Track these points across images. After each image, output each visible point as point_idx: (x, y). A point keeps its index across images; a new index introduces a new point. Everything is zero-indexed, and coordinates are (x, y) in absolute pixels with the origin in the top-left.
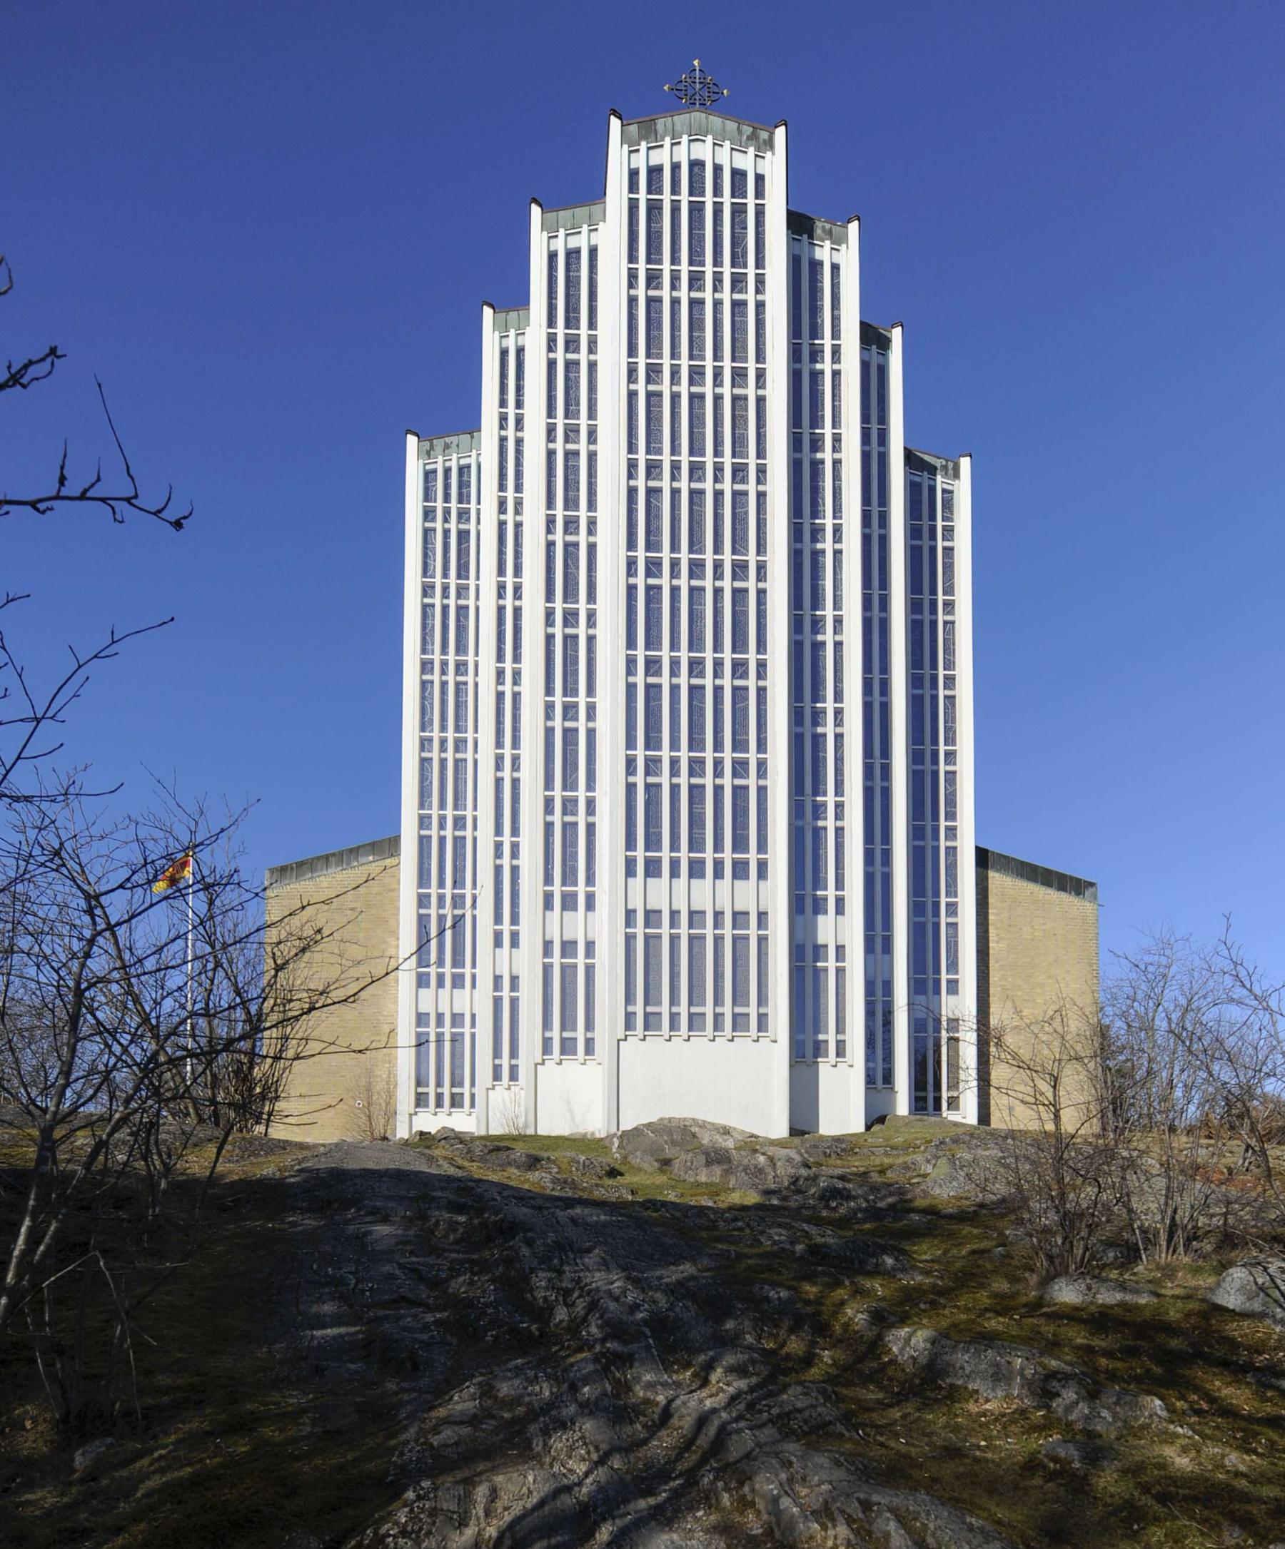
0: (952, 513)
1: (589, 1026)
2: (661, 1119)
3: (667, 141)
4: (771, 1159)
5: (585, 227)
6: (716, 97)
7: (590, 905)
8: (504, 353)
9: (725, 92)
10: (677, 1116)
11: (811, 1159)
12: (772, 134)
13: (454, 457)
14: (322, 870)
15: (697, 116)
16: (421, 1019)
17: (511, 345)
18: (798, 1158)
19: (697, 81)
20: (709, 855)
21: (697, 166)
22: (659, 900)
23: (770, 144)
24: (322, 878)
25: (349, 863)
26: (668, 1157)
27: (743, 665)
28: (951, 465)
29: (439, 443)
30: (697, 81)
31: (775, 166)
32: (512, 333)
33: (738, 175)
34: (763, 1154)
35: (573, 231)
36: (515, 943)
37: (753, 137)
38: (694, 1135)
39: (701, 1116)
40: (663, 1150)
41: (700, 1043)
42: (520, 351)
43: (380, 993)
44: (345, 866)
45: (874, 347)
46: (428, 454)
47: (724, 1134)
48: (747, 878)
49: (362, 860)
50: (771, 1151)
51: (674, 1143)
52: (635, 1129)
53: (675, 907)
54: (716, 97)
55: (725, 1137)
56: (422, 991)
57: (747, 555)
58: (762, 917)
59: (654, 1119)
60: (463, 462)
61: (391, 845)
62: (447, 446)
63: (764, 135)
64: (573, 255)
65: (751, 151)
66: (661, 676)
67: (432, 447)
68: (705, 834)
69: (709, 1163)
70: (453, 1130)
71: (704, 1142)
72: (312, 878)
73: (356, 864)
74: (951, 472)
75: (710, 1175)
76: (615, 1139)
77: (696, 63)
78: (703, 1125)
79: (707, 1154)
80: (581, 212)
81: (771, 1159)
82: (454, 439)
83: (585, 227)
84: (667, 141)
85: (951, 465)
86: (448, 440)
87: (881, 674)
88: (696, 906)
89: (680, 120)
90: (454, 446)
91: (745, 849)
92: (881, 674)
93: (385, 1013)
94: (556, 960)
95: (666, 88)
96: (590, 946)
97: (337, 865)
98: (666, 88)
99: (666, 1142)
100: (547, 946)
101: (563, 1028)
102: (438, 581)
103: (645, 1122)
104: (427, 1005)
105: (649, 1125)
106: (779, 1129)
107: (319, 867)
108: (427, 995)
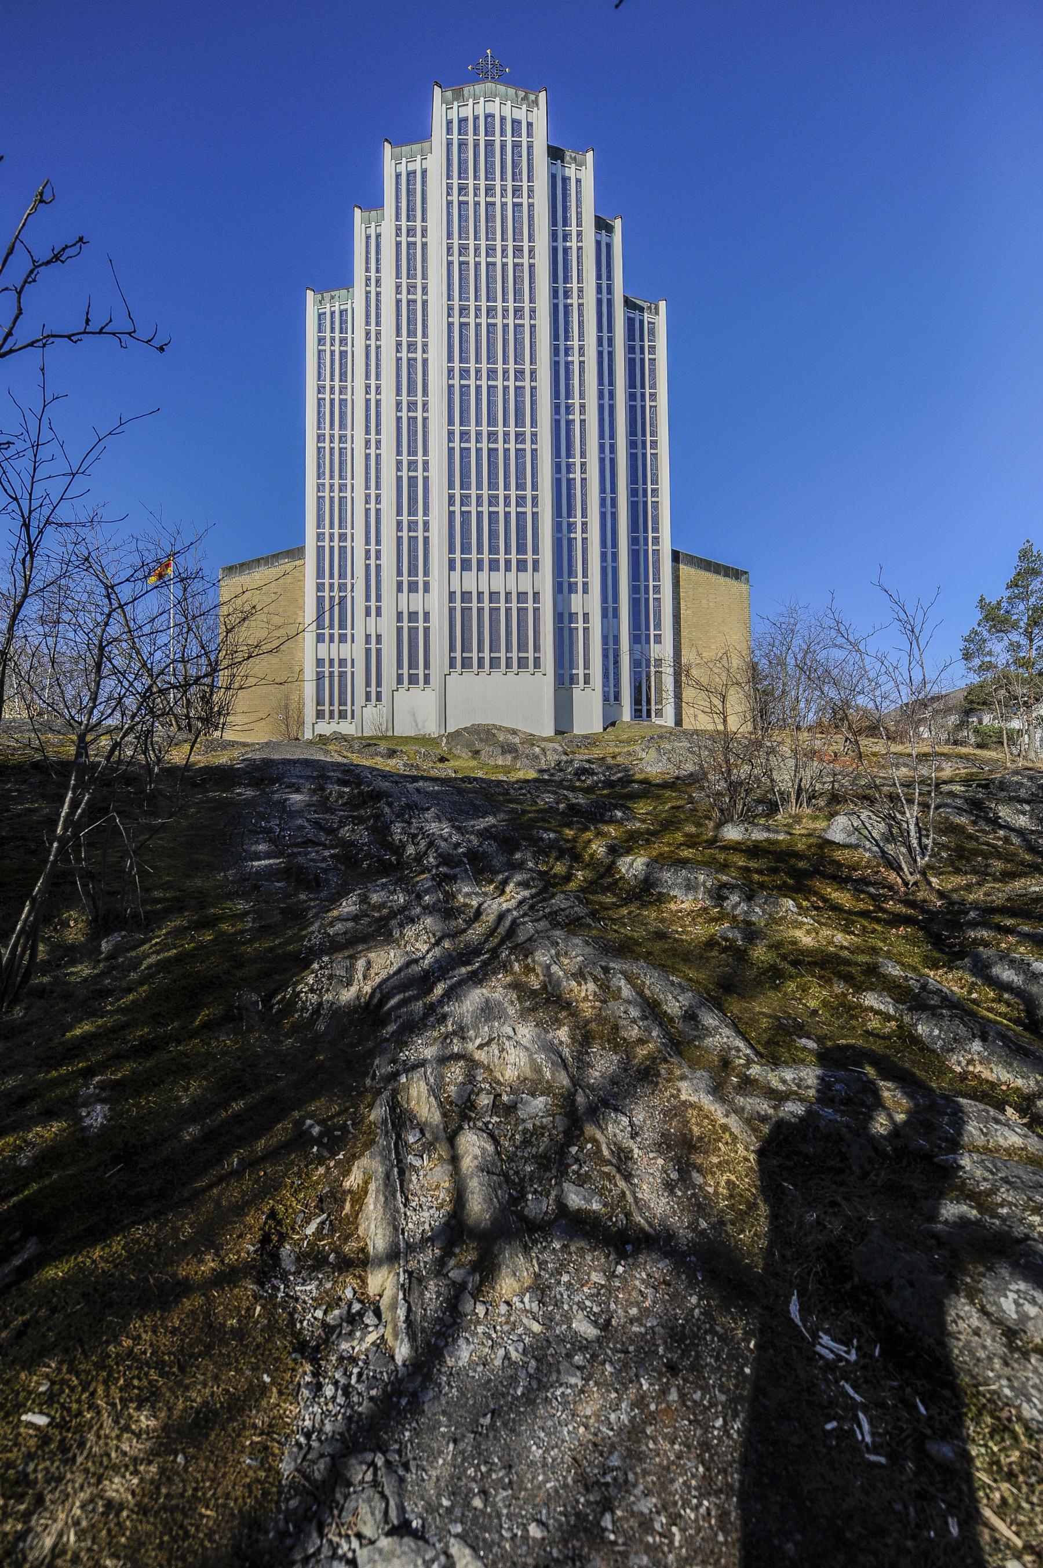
5: (419, 158)
12: (537, 97)
16: (320, 662)
17: (372, 231)
23: (536, 103)
31: (540, 117)
35: (411, 159)
36: (378, 614)
41: (497, 675)
61: (297, 553)
62: (332, 297)
63: (532, 97)
65: (524, 107)
78: (500, 728)
94: (405, 624)
96: (427, 615)
101: (410, 668)
104: (323, 654)
108: (323, 648)
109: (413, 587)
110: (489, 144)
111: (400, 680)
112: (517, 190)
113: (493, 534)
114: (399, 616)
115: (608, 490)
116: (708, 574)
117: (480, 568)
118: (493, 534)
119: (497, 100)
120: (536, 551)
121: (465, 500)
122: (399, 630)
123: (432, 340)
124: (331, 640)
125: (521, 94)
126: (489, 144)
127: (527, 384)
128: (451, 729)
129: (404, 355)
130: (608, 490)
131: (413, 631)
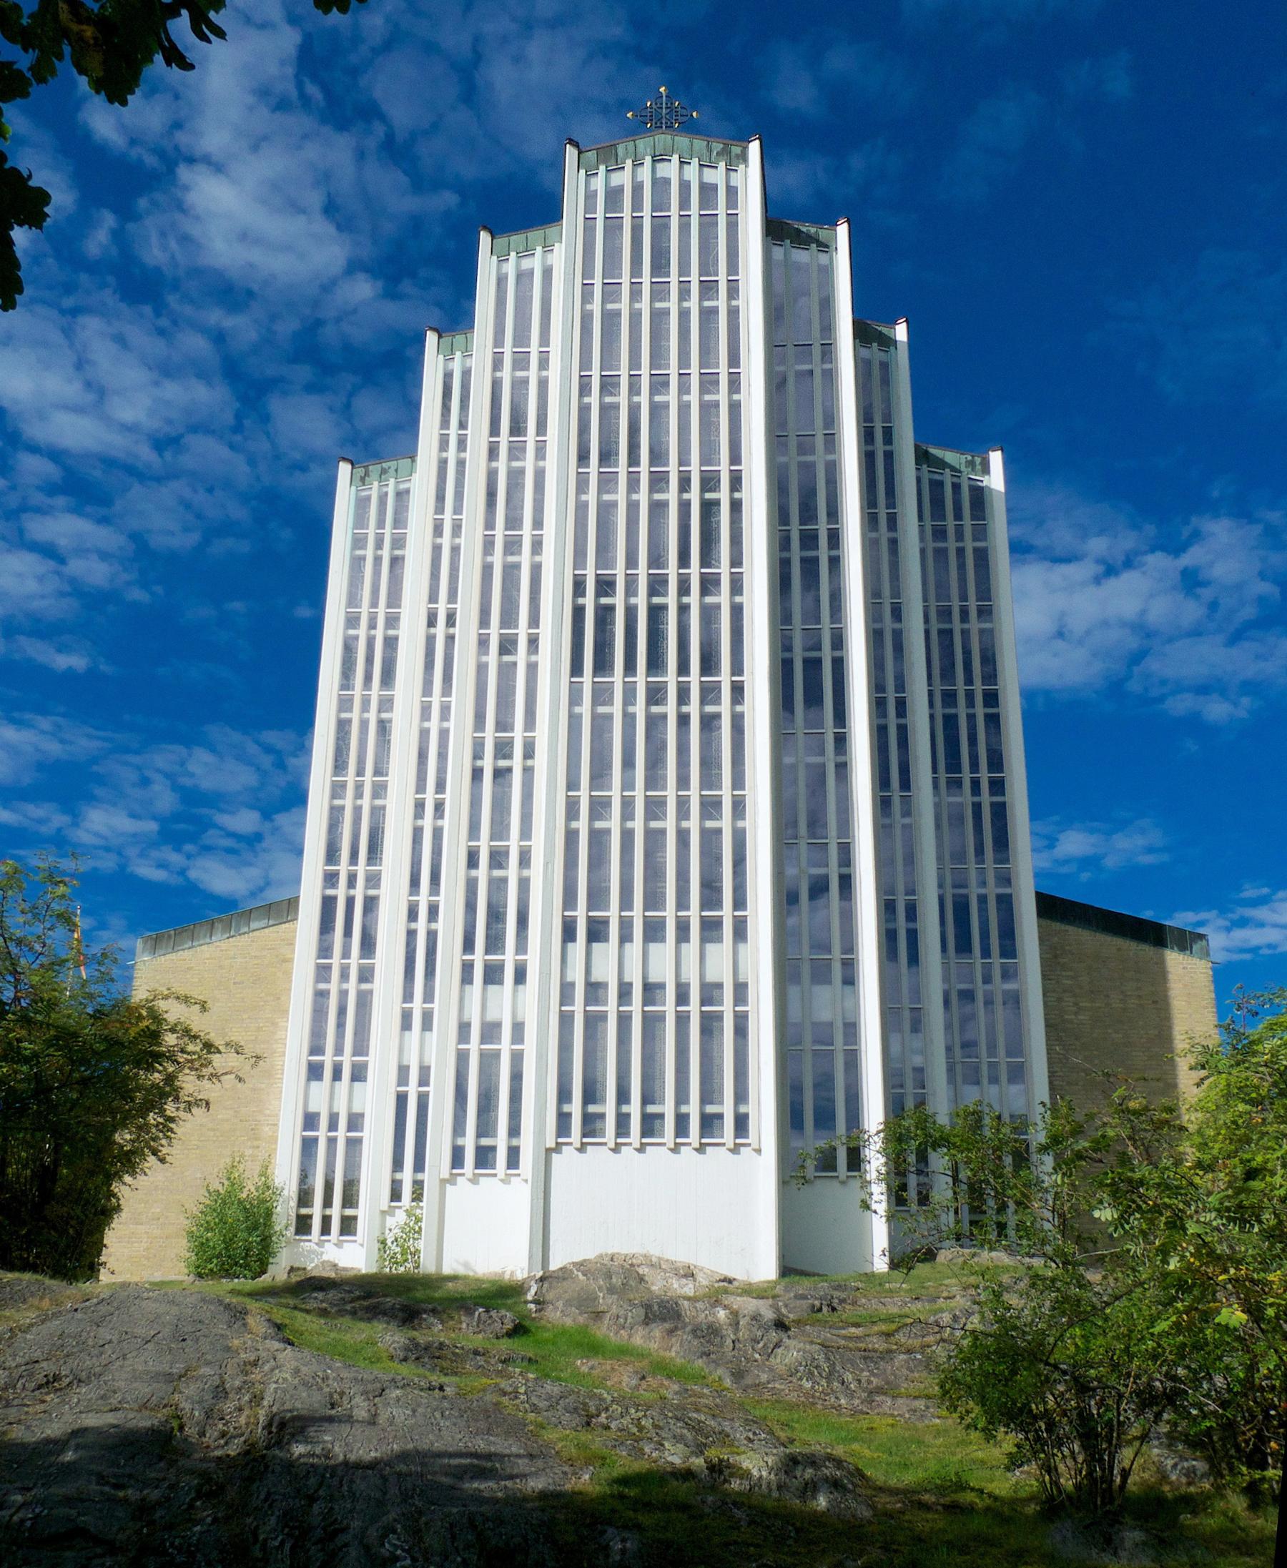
0: (983, 511)
1: (514, 1131)
2: (601, 1256)
3: (629, 163)
4: (735, 1315)
5: (539, 249)
6: (685, 119)
7: (520, 976)
8: (448, 376)
9: (694, 114)
10: (625, 1251)
11: (791, 1316)
12: (745, 149)
13: (392, 481)
14: (205, 936)
15: (663, 139)
16: (310, 1121)
17: (456, 367)
18: (769, 1315)
19: (664, 106)
20: (669, 913)
21: (661, 185)
22: (663, 971)
23: (744, 157)
24: (205, 948)
25: (238, 929)
26: (601, 1309)
27: (713, 690)
28: (978, 460)
29: (375, 469)
30: (664, 106)
31: (750, 177)
32: (458, 354)
33: (708, 191)
34: (725, 1307)
35: (527, 252)
36: (427, 1024)
37: (725, 152)
38: (641, 1279)
39: (655, 1251)
40: (596, 1298)
41: (658, 1155)
42: (466, 374)
43: (263, 1086)
44: (232, 933)
45: (875, 345)
46: (363, 480)
47: (685, 1276)
48: (663, 940)
49: (254, 925)
50: (738, 1302)
51: (611, 1290)
52: (561, 1269)
53: (653, 978)
54: (685, 119)
55: (684, 1281)
56: (314, 1084)
57: (719, 568)
58: (741, 991)
59: (591, 1255)
60: (402, 486)
61: (288, 908)
62: (384, 471)
63: (736, 150)
64: (524, 277)
65: (722, 165)
66: (612, 704)
67: (367, 474)
68: (665, 887)
69: (647, 1321)
70: (335, 1265)
71: (654, 1288)
72: (192, 947)
73: (246, 929)
74: (978, 467)
75: (648, 1338)
76: (533, 1283)
77: (662, 89)
78: (656, 1265)
79: (648, 1307)
80: (535, 235)
81: (735, 1315)
82: (393, 464)
83: (539, 249)
84: (629, 163)
85: (978, 460)
86: (384, 465)
87: (897, 692)
88: (711, 977)
89: (643, 144)
90: (392, 471)
91: (718, 904)
92: (897, 692)
93: (268, 1112)
94: (474, 1046)
95: (629, 115)
96: (518, 1029)
97: (224, 931)
98: (629, 115)
99: (600, 1289)
100: (464, 1029)
101: (480, 1134)
102: (365, 610)
103: (577, 1259)
104: (319, 1104)
105: (581, 1265)
106: (765, 1268)
107: (201, 935)
108: (320, 1091)
109: (493, 975)
110: (659, 317)
111: (457, 1158)
112: (708, 289)
113: (654, 872)
114: (464, 1030)
115: (886, 591)
116: (1119, 942)
117: (625, 937)
118: (654, 872)
119: (675, 158)
120: (739, 902)
121: (599, 808)
122: (462, 1058)
123: (542, 735)
124: (337, 1075)
125: (718, 147)
126: (659, 317)
127: (723, 598)
128: (554, 1265)
129: (482, 873)
130: (886, 591)
131: (489, 1062)
